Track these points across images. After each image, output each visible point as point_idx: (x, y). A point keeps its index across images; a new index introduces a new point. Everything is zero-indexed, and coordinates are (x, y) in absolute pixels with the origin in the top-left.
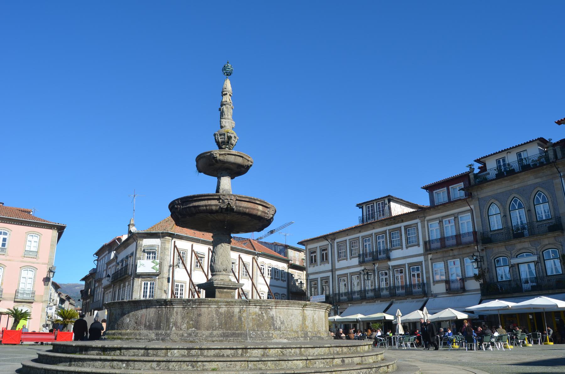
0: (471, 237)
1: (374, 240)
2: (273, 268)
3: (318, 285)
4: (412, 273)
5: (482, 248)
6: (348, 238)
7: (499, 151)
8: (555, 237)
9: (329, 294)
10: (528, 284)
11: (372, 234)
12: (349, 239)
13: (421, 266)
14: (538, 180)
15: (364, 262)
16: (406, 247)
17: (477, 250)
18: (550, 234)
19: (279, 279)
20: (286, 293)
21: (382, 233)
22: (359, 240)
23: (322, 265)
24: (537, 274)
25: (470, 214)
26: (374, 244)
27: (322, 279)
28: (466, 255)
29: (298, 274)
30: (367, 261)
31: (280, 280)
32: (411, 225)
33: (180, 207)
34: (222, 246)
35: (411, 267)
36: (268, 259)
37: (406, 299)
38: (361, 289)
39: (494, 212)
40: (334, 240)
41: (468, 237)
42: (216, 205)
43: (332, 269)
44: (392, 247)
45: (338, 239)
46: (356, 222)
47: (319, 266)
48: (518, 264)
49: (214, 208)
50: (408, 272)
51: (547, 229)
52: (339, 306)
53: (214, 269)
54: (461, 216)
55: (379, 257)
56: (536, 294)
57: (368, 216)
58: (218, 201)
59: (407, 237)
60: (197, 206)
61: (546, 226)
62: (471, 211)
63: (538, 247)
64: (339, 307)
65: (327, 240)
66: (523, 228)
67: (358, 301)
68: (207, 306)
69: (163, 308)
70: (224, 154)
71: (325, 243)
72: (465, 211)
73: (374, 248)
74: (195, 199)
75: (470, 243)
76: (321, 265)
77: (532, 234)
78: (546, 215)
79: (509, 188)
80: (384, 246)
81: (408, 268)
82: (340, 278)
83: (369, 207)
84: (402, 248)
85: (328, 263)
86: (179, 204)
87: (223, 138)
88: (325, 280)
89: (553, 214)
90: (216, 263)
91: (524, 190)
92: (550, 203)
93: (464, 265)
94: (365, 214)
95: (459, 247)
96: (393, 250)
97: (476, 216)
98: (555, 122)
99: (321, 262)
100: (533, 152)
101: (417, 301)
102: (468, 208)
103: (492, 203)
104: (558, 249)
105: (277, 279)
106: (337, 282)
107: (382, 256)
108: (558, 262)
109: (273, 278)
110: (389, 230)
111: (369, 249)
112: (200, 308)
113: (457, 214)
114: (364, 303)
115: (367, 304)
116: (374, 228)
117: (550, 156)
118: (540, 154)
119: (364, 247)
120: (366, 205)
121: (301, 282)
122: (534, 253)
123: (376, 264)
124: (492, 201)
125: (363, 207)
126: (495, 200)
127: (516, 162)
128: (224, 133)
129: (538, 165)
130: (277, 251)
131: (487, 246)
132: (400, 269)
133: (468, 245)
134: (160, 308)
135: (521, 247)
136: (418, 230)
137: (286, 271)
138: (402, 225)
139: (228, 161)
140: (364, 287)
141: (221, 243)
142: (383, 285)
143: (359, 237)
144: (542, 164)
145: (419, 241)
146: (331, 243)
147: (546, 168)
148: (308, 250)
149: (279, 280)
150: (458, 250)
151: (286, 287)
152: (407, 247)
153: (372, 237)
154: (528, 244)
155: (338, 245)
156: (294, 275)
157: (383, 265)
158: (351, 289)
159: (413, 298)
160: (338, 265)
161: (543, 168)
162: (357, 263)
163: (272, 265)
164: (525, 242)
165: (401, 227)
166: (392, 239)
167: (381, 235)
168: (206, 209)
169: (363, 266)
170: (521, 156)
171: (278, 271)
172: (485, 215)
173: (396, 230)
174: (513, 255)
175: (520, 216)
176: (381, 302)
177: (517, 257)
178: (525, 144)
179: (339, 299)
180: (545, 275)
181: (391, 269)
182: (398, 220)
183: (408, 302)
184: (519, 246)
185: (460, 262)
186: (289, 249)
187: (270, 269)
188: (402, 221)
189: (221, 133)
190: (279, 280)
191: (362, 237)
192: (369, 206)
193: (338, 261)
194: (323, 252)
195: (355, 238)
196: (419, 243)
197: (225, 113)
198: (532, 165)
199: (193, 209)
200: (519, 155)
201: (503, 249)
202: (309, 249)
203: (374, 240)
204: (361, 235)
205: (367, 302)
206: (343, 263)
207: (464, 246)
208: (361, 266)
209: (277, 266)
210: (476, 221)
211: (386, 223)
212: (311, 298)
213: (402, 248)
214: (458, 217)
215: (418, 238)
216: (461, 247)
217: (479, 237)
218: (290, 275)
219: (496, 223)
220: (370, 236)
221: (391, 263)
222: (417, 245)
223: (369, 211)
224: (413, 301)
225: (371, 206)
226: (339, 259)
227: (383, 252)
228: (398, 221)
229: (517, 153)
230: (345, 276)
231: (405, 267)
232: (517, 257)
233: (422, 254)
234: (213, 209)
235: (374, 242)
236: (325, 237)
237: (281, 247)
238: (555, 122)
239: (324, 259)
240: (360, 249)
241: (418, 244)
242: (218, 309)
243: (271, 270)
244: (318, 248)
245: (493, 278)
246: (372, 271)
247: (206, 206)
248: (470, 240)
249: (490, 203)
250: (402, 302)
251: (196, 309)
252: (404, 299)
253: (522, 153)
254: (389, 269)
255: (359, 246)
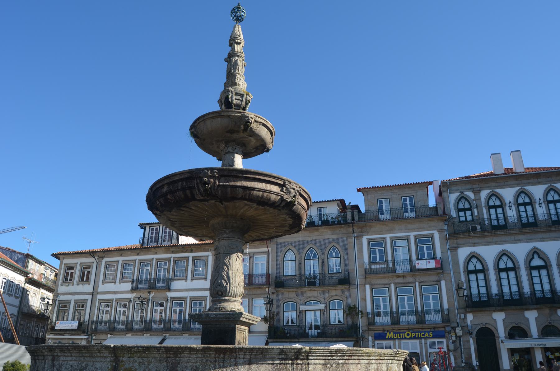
0: (263, 278)
1: (154, 266)
2: (8, 280)
3: (69, 309)
4: (193, 308)
5: (274, 291)
6: (121, 259)
7: (317, 201)
8: (342, 289)
9: (84, 321)
10: (312, 331)
11: (152, 260)
12: (123, 260)
13: (205, 301)
14: (334, 236)
15: (155, 288)
16: (191, 279)
17: (267, 293)
18: (340, 287)
19: (12, 295)
20: (16, 314)
21: (165, 260)
22: (135, 263)
23: (81, 286)
24: (322, 321)
25: (266, 256)
26: (153, 270)
27: (76, 302)
28: (255, 296)
29: (34, 291)
30: (142, 288)
31: (13, 296)
32: (201, 256)
33: (215, 182)
34: (238, 256)
35: (193, 301)
36: (6, 267)
37: (182, 335)
38: (111, 319)
39: (290, 258)
40: (103, 258)
41: (262, 278)
42: (277, 194)
43: (93, 292)
44: (174, 277)
45: (107, 257)
46: (135, 243)
47: (75, 286)
48: (305, 311)
49: (273, 197)
50: (190, 307)
51: (338, 281)
52: (95, 335)
53: (228, 291)
54: (256, 256)
55: (157, 285)
56: (321, 340)
57: (149, 238)
58: (279, 188)
59: (194, 269)
60: (250, 188)
61: (337, 278)
62: (268, 253)
63: (326, 297)
64: (94, 337)
65: (94, 257)
66: (315, 277)
67: (122, 332)
68: (356, 361)
69: (289, 364)
70: (260, 122)
71: (90, 259)
72: (261, 252)
73: (153, 275)
74: (248, 176)
75: (263, 285)
76: (78, 285)
77: (323, 284)
78: (336, 269)
79: (307, 239)
80: (164, 275)
81: (190, 302)
82: (101, 304)
83: (153, 229)
84: (186, 280)
85: (89, 284)
86: (213, 177)
87: (240, 100)
88: (80, 305)
89: (343, 269)
90: (231, 282)
91: (320, 243)
92: (342, 258)
93: (252, 306)
94: (146, 235)
95: (250, 287)
96: (175, 280)
97: (358, 265)
98: (357, 189)
99: (64, 282)
100: (333, 211)
101: (195, 339)
102: (266, 250)
103: (289, 249)
104: (343, 301)
105: (10, 295)
106: (97, 307)
107: (161, 285)
108: (341, 312)
109: (6, 293)
110: (174, 258)
111: (146, 275)
112: (348, 365)
113: (253, 254)
114: (129, 335)
115: (133, 337)
116: (156, 253)
117: (348, 217)
118: (338, 213)
119: (140, 271)
120: (150, 227)
121: (48, 302)
122: (321, 302)
123: (152, 293)
124: (290, 247)
125: (145, 227)
126: (292, 247)
127: (316, 216)
128: (243, 93)
129: (336, 223)
130: (13, 259)
131: (279, 290)
132: (180, 301)
133: (260, 286)
134: (280, 364)
135: (310, 295)
136: (208, 263)
137: (22, 285)
138: (191, 255)
139: (259, 134)
140: (132, 316)
141: (237, 252)
142: (157, 316)
143: (135, 260)
144: (339, 223)
145: (207, 275)
146: (98, 261)
147: (344, 227)
148: (63, 265)
149: (12, 296)
150: (248, 290)
151: (18, 305)
152: (192, 280)
153: (152, 262)
154: (318, 293)
155: (106, 265)
156: (29, 292)
157: (160, 295)
158: (114, 317)
159: (191, 335)
160: (101, 288)
161: (342, 226)
162: (129, 289)
163: (8, 276)
164: (315, 290)
165: (188, 257)
166: (176, 268)
167: (163, 262)
168: (263, 195)
169: (135, 293)
170: (321, 212)
171: (13, 285)
172: (281, 259)
173: (182, 259)
174: (302, 302)
175: (313, 266)
176: (151, 336)
177: (305, 304)
178: (328, 201)
179: (96, 328)
180: (329, 324)
181: (169, 300)
182: (187, 249)
183: (184, 338)
184: (309, 294)
185: (249, 302)
186: (31, 259)
187: (5, 281)
188: (191, 251)
189: (239, 92)
190: (12, 296)
191: (140, 260)
192: (154, 228)
193: (103, 283)
194: (83, 270)
195: (131, 260)
196: (207, 277)
197: (239, 68)
198: (331, 222)
199: (240, 190)
200: (320, 210)
201: (293, 295)
202: (65, 264)
203: (154, 266)
204: (138, 258)
205: (133, 335)
206: (110, 287)
207: (256, 287)
208: (133, 293)
209: (13, 278)
210: (272, 265)
211: (172, 250)
212: (58, 323)
213: (186, 280)
214: (253, 257)
215: (206, 271)
216: (253, 287)
217: (272, 280)
218: (25, 291)
219: (290, 269)
220: (150, 261)
221: (170, 294)
222: (204, 279)
223: (152, 234)
224: (191, 338)
225: (156, 228)
226: (104, 282)
227: (146, 280)
228: (187, 250)
229: (318, 208)
230: (110, 302)
231: (187, 301)
232: (305, 304)
233: (208, 288)
234: (272, 198)
235: (154, 268)
236: (92, 254)
237: (20, 256)
238: (357, 189)
239: (84, 278)
240: (134, 274)
241: (206, 278)
242: (368, 366)
243: (5, 282)
244: (78, 265)
245: (280, 322)
246: (146, 300)
247: (264, 191)
248: (263, 282)
249: (288, 249)
250: (178, 338)
251: (342, 366)
252: (179, 335)
253: (322, 209)
254: (168, 300)
255: (135, 270)
